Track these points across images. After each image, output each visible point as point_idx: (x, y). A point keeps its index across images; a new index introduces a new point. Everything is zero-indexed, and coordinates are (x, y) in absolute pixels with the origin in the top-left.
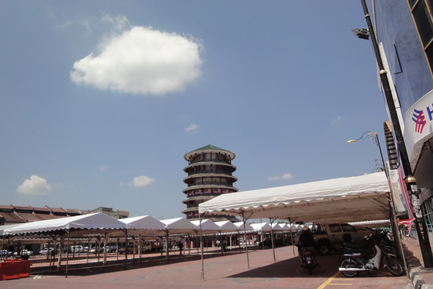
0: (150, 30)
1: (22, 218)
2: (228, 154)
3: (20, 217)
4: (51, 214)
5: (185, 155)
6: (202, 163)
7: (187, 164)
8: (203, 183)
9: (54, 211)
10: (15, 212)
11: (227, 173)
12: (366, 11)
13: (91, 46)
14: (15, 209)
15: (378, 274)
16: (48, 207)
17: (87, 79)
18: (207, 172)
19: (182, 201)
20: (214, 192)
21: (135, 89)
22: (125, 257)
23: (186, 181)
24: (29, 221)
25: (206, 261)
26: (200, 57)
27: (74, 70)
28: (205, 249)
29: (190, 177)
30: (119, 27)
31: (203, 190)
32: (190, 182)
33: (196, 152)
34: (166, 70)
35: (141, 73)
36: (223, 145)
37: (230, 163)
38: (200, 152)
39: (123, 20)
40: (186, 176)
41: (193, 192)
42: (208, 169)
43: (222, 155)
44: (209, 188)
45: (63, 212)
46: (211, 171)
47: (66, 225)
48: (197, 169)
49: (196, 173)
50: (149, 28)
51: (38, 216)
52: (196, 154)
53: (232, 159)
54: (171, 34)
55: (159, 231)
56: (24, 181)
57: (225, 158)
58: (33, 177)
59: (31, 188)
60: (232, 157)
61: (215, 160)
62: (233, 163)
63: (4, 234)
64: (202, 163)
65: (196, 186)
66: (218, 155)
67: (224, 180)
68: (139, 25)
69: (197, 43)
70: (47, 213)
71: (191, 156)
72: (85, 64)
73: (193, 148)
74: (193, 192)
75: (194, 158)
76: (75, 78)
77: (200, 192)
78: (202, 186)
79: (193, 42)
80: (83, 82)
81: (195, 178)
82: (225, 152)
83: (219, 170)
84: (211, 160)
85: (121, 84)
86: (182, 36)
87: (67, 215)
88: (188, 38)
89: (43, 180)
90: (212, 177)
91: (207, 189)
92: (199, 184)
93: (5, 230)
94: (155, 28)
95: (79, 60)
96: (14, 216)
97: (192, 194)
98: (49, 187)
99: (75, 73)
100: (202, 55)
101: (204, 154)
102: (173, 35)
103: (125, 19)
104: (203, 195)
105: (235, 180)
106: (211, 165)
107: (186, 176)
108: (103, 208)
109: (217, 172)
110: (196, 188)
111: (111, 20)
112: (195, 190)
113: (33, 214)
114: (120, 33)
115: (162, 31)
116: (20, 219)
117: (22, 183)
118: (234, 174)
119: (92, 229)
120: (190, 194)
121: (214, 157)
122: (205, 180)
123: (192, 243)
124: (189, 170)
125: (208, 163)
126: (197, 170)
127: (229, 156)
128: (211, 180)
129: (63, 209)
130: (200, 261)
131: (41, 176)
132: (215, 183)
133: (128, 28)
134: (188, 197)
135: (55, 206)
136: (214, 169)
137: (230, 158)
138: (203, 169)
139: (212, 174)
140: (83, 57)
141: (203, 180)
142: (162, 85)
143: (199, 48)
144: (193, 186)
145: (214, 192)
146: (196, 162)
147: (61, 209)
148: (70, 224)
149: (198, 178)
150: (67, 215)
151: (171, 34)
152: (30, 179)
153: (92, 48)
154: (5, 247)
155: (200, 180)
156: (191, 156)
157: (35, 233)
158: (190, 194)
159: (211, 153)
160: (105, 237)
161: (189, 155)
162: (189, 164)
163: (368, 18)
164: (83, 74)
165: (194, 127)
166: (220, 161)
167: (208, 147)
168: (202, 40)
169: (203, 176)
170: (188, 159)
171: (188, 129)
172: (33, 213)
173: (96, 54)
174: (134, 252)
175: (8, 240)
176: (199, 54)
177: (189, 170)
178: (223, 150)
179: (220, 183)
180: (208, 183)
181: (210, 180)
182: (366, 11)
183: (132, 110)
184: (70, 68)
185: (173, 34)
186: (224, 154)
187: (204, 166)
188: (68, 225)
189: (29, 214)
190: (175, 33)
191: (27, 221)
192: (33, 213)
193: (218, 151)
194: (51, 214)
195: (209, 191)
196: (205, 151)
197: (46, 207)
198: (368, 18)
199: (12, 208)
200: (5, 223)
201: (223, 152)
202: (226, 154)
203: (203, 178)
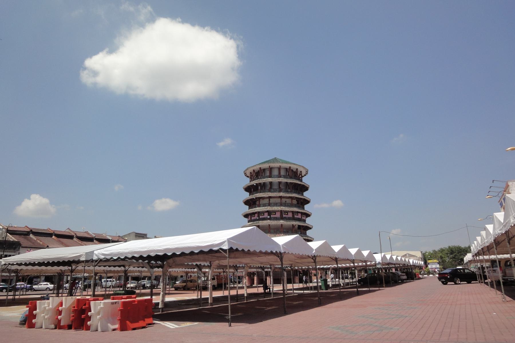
0: (179, 22)
1: (41, 243)
2: (300, 169)
3: (39, 241)
4: (75, 239)
5: (246, 170)
6: (270, 180)
7: (247, 182)
8: (269, 205)
9: (78, 235)
10: (31, 236)
11: (299, 193)
13: (107, 41)
14: (32, 232)
16: (71, 231)
17: (100, 79)
18: (275, 191)
20: (284, 216)
21: (159, 94)
23: (247, 202)
24: (50, 247)
26: (238, 57)
27: (85, 69)
28: (290, 286)
29: (250, 198)
30: (142, 18)
31: (269, 213)
32: (250, 203)
34: (197, 72)
35: (165, 74)
37: (301, 181)
38: (266, 166)
39: (146, 10)
40: (247, 196)
41: (256, 215)
42: (275, 187)
44: (278, 211)
45: (89, 236)
47: (80, 256)
48: (262, 187)
49: (260, 193)
50: (177, 19)
51: (60, 241)
52: (290, 167)
54: (204, 28)
55: (302, 257)
56: (23, 201)
57: (295, 174)
58: (33, 196)
59: (31, 209)
61: (285, 177)
62: (306, 180)
63: (95, 258)
64: (270, 180)
65: (261, 208)
66: (287, 170)
67: (295, 202)
68: (165, 17)
69: (235, 40)
70: (71, 237)
71: (254, 171)
72: (98, 62)
73: (256, 160)
74: (256, 215)
75: (257, 174)
76: (86, 78)
77: (266, 215)
78: (269, 208)
79: (231, 39)
80: (95, 84)
81: (260, 198)
83: (289, 188)
84: (279, 176)
85: (142, 87)
86: (217, 31)
87: (95, 241)
88: (224, 33)
89: (45, 201)
90: (281, 197)
91: (275, 212)
92: (264, 205)
93: (95, 252)
94: (184, 21)
95: (91, 57)
96: (30, 240)
97: (256, 217)
98: (52, 209)
99: (86, 72)
100: (241, 55)
101: (271, 169)
102: (207, 30)
103: (149, 8)
104: (270, 219)
105: (307, 202)
107: (247, 196)
108: (136, 233)
109: (286, 191)
110: (262, 210)
111: (132, 9)
113: (54, 239)
114: (142, 25)
115: (193, 25)
116: (39, 244)
117: (20, 204)
118: (306, 195)
119: (255, 251)
120: (253, 218)
121: (283, 173)
122: (272, 201)
123: (255, 278)
124: (249, 189)
125: (275, 180)
126: (261, 189)
127: (301, 172)
129: (88, 234)
131: (43, 194)
132: (285, 205)
133: (152, 20)
135: (80, 229)
139: (282, 194)
140: (96, 53)
141: (269, 200)
142: (191, 90)
143: (238, 47)
144: (257, 208)
145: (284, 216)
146: (261, 178)
147: (87, 232)
148: (229, 240)
149: (263, 198)
150: (95, 241)
151: (204, 28)
152: (29, 198)
153: (108, 43)
154: (4, 281)
155: (266, 201)
156: (254, 171)
157: (141, 257)
158: (253, 218)
159: (279, 169)
160: (211, 266)
161: (251, 170)
164: (95, 73)
165: (228, 141)
166: (291, 178)
167: (275, 160)
168: (242, 37)
169: (270, 195)
170: (249, 175)
171: (221, 144)
172: (53, 237)
173: (113, 50)
175: (70, 268)
176: (238, 53)
177: (249, 189)
178: (294, 164)
179: (291, 205)
180: (276, 204)
181: (278, 200)
183: (155, 121)
184: (80, 66)
185: (206, 28)
186: (295, 170)
188: (226, 243)
189: (49, 238)
190: (209, 28)
191: (48, 246)
192: (53, 237)
193: (287, 166)
194: (75, 239)
195: (278, 215)
196: (272, 165)
197: (68, 231)
199: (28, 230)
200: (21, 249)
201: (294, 167)
202: (297, 169)
203: (270, 197)
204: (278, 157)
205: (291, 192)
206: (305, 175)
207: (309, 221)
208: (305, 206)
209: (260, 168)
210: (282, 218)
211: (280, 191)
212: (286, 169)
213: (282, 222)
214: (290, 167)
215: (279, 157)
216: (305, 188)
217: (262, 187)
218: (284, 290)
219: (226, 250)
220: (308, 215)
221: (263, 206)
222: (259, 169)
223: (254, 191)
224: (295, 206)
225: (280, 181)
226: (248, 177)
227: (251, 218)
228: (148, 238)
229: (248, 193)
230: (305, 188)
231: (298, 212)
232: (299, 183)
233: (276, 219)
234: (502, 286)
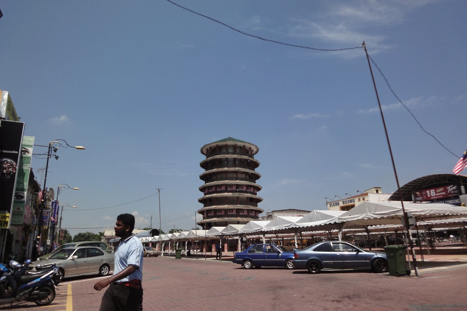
2: (247, 146)
7: (203, 158)
12: (45, 179)
15: (336, 250)
23: (202, 189)
36: (243, 136)
37: (253, 158)
40: (203, 171)
41: (207, 190)
42: (231, 150)
52: (244, 146)
53: (256, 152)
57: (245, 150)
60: (255, 150)
62: (256, 158)
73: (214, 139)
75: (211, 151)
82: (250, 146)
92: (231, 179)
101: (227, 146)
107: (203, 171)
118: (257, 171)
120: (210, 191)
124: (204, 165)
138: (220, 163)
139: (237, 169)
158: (210, 191)
161: (208, 147)
163: (46, 177)
167: (230, 139)
170: (205, 151)
177: (204, 165)
182: (45, 179)
186: (248, 149)
198: (46, 177)
204: (231, 137)
205: (245, 167)
207: (259, 195)
208: (256, 181)
215: (232, 136)
216: (255, 165)
217: (220, 163)
220: (258, 189)
226: (203, 154)
227: (208, 190)
229: (204, 182)
230: (255, 165)
231: (252, 210)
232: (251, 159)
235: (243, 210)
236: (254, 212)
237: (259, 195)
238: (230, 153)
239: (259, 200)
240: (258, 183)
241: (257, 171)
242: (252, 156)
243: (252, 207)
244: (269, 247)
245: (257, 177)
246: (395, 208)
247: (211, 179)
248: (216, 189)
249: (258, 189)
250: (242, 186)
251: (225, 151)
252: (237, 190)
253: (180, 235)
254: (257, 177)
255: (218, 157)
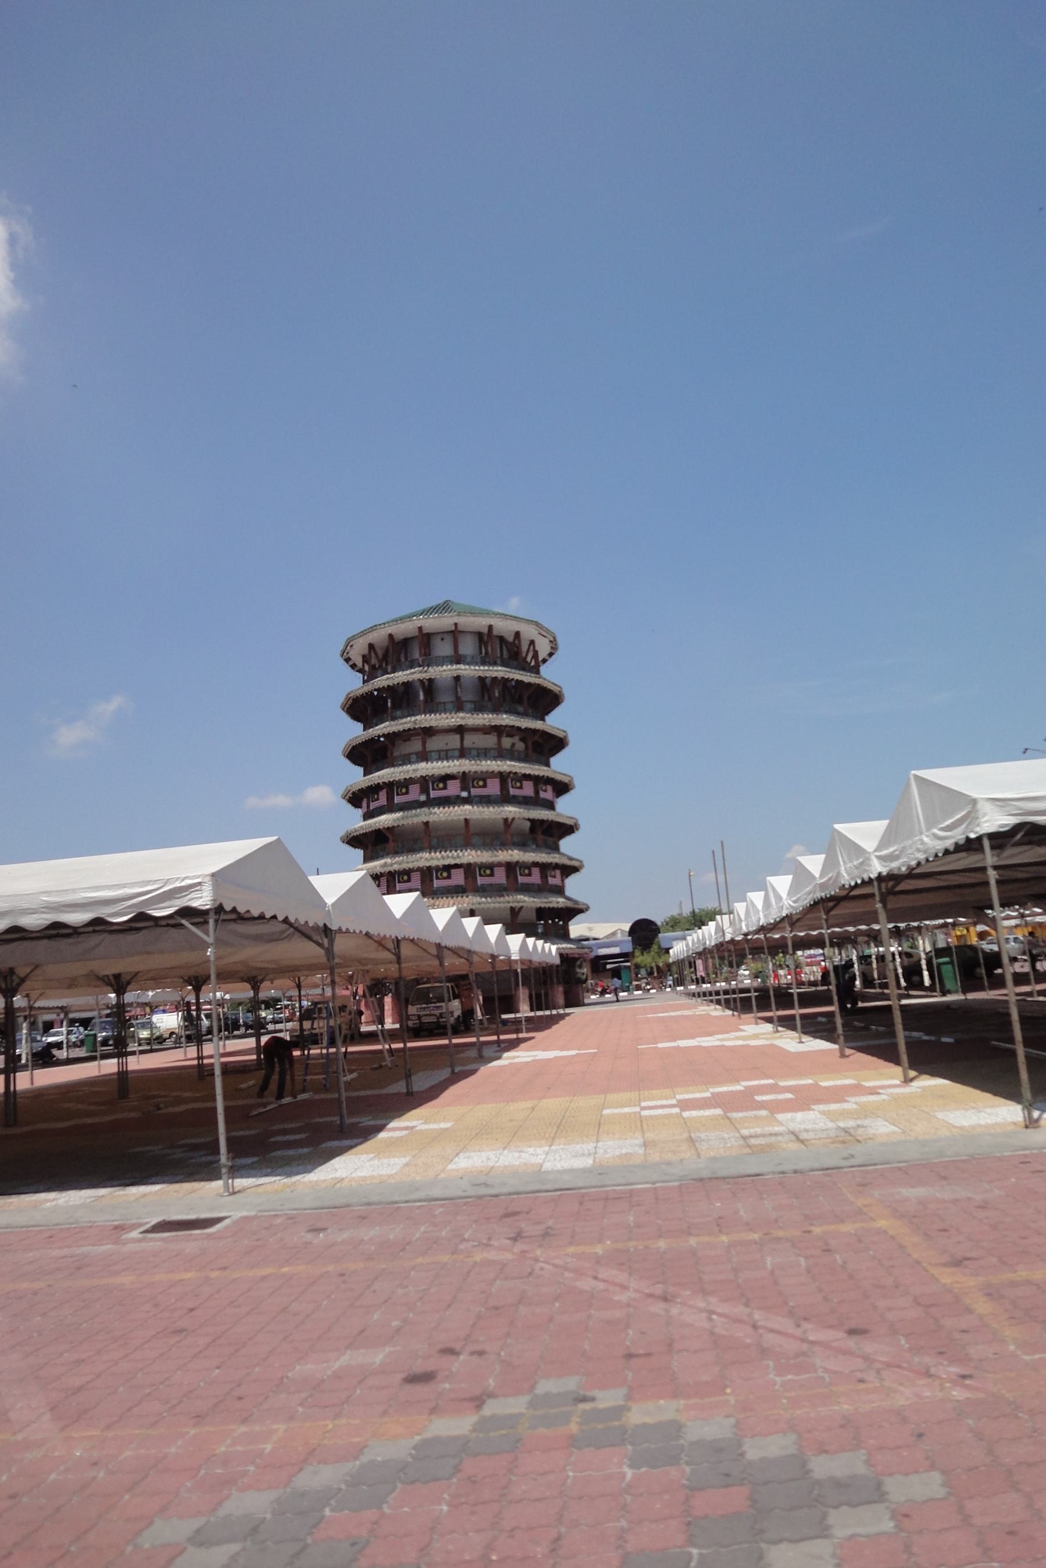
2: (529, 632)
7: (354, 683)
19: (342, 833)
22: (253, 1039)
23: (356, 798)
25: (142, 1056)
26: (14, 282)
32: (365, 755)
33: (390, 630)
38: (408, 629)
40: (355, 731)
43: (502, 639)
46: (459, 706)
48: (403, 698)
52: (391, 636)
53: (544, 661)
57: (510, 649)
60: (543, 647)
62: (550, 675)
71: (371, 646)
73: (393, 604)
75: (394, 651)
77: (415, 794)
82: (515, 626)
84: (458, 659)
92: (445, 755)
101: (425, 639)
106: (457, 678)
107: (355, 731)
110: (402, 777)
112: (390, 786)
118: (555, 721)
120: (373, 805)
121: (468, 647)
122: (470, 740)
124: (361, 708)
125: (442, 672)
127: (532, 642)
128: (458, 745)
130: (96, 1063)
134: (367, 816)
136: (467, 696)
137: (536, 654)
155: (416, 745)
161: (360, 648)
162: (364, 682)
167: (444, 607)
170: (359, 662)
174: (446, 999)
177: (361, 708)
180: (483, 753)
187: (429, 686)
193: (481, 623)
201: (504, 628)
202: (517, 635)
206: (551, 655)
209: (420, 628)
210: (506, 799)
211: (459, 707)
212: (480, 635)
213: (510, 811)
214: (490, 627)
217: (403, 698)
218: (200, 1058)
219: (206, 913)
220: (562, 788)
221: (440, 759)
222: (386, 643)
223: (395, 706)
224: (525, 759)
225: (481, 674)
227: (368, 806)
228: (529, 819)
229: (360, 770)
230: (546, 699)
233: (486, 801)
234: (1024, 1075)
235: (491, 867)
236: (536, 871)
237: (565, 808)
238: (441, 661)
239: (568, 829)
240: (560, 765)
241: (555, 721)
242: (536, 670)
243: (543, 857)
244: (781, 972)
245: (555, 744)
246: (148, 883)
247: (385, 757)
248: (390, 798)
249: (562, 788)
250: (483, 778)
251: (416, 655)
252: (464, 794)
253: (720, 930)
254: (555, 744)
255: (401, 676)
